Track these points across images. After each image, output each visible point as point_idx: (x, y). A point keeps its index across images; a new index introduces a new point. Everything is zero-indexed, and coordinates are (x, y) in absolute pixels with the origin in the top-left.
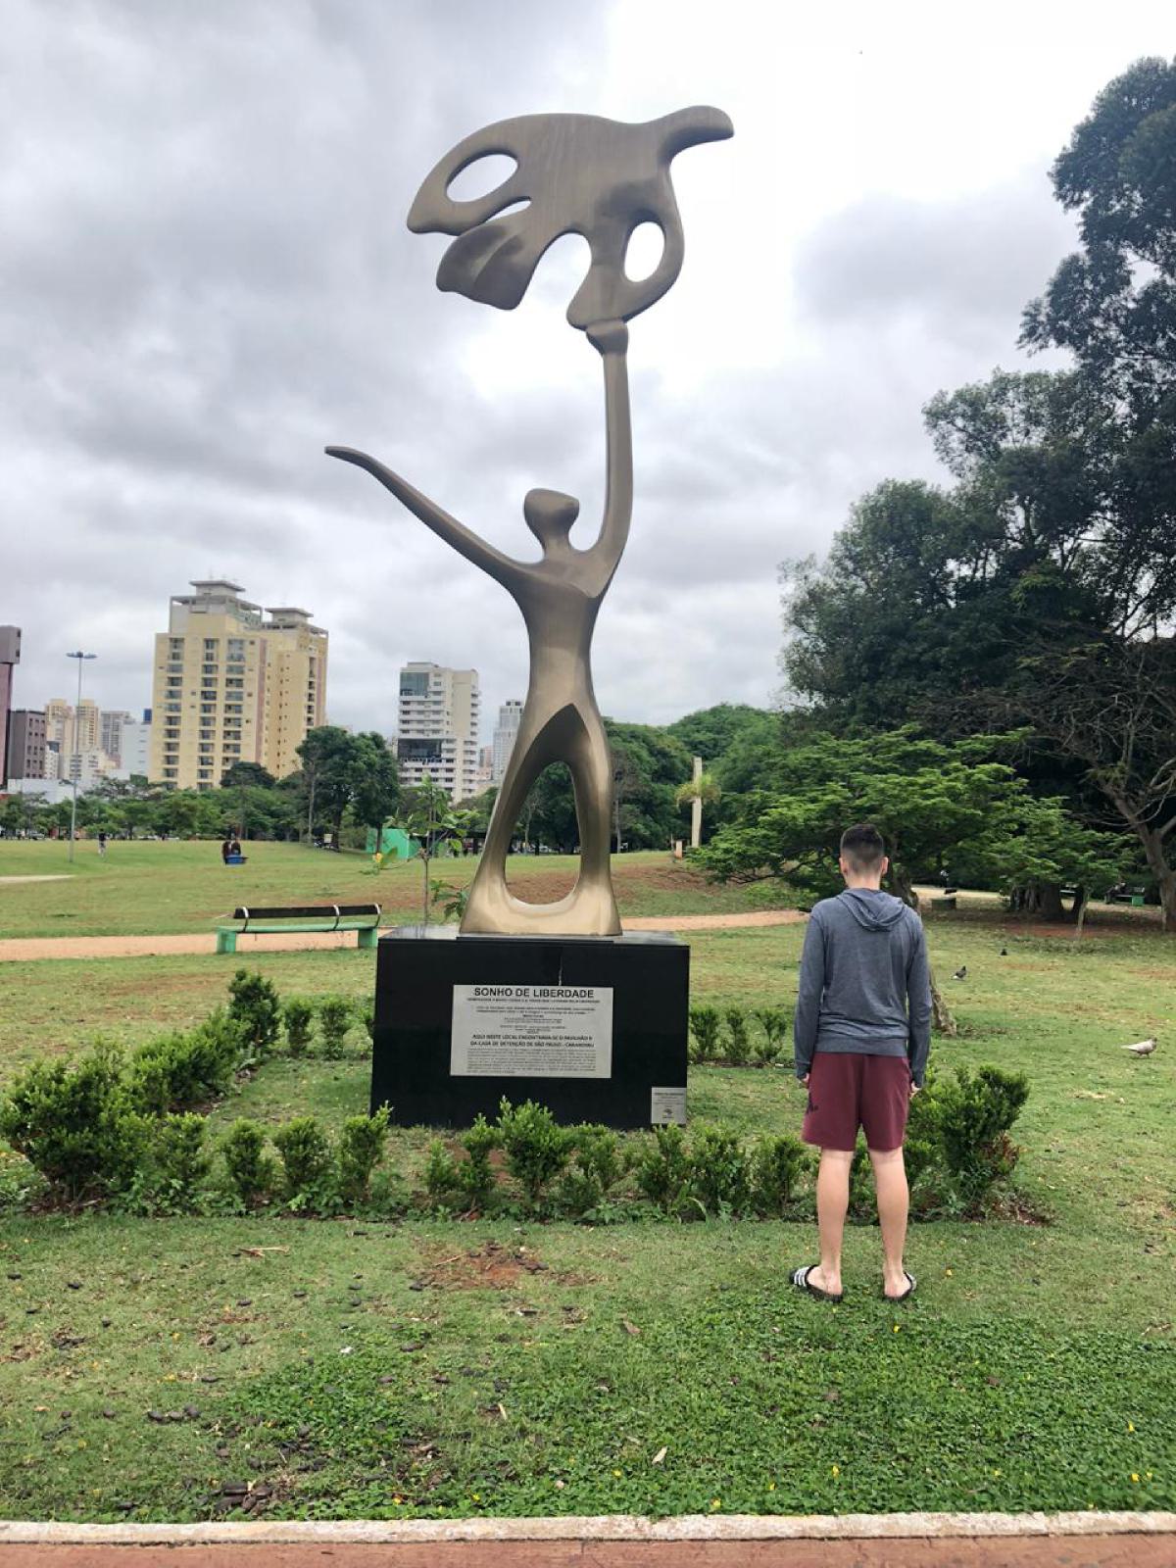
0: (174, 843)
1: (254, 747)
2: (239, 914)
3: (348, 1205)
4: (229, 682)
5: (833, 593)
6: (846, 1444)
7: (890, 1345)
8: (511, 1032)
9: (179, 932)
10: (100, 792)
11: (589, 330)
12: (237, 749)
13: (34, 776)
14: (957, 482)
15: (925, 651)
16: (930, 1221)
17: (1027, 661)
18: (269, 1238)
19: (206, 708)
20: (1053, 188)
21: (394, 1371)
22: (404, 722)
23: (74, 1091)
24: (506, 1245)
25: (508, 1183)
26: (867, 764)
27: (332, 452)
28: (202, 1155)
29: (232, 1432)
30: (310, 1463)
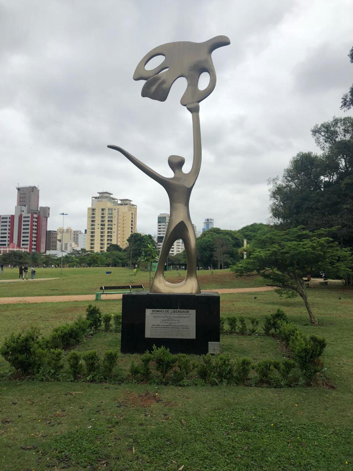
0: (92, 269)
1: (116, 240)
2: (101, 288)
3: (105, 379)
4: (109, 221)
5: (285, 187)
6: (246, 466)
7: (270, 430)
8: (164, 324)
9: (87, 294)
10: (72, 254)
11: (187, 106)
12: (111, 240)
13: (54, 250)
14: (322, 152)
15: (313, 204)
16: (294, 387)
17: (345, 206)
18: (78, 390)
19: (102, 229)
21: (102, 435)
22: (159, 231)
23: (23, 342)
24: (151, 393)
25: (154, 372)
26: (287, 238)
27: (110, 147)
28: (61, 362)
29: (44, 454)
30: (66, 466)
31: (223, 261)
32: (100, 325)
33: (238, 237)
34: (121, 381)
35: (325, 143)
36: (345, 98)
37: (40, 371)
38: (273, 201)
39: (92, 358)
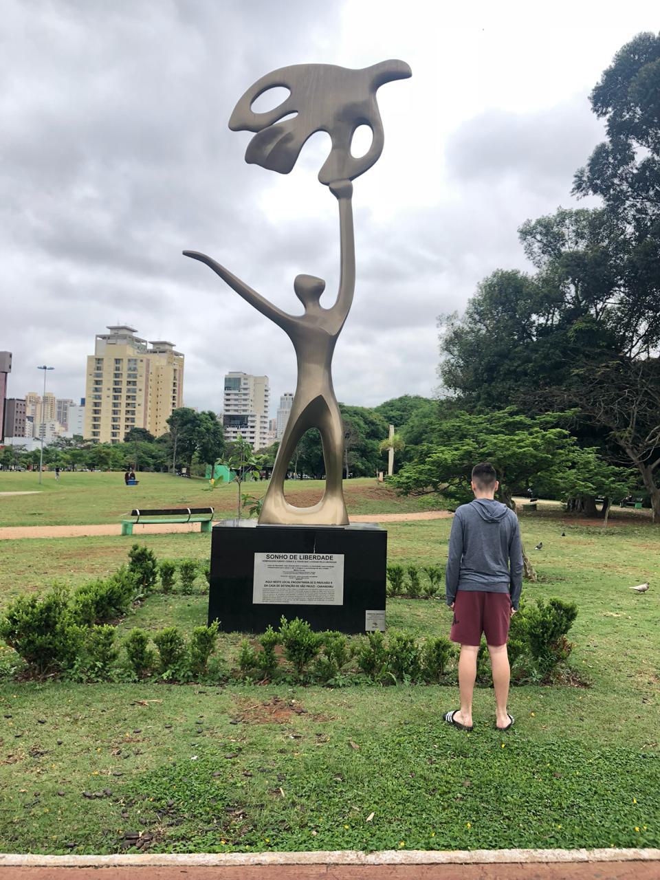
0: (97, 473)
1: (143, 419)
2: (134, 513)
3: (195, 676)
5: (468, 333)
6: (475, 810)
8: (287, 579)
10: (56, 445)
12: (133, 420)
13: (19, 436)
15: (519, 366)
16: (522, 685)
18: (152, 695)
19: (116, 398)
20: (591, 106)
21: (221, 769)
22: (227, 405)
23: (41, 612)
24: (284, 699)
26: (487, 429)
27: (186, 254)
28: (113, 648)
29: (130, 804)
30: (174, 821)
31: (348, 464)
32: (154, 582)
33: (375, 421)
34: (224, 681)
35: (542, 255)
36: (580, 175)
37: (75, 664)
38: (446, 356)
39: (171, 641)
